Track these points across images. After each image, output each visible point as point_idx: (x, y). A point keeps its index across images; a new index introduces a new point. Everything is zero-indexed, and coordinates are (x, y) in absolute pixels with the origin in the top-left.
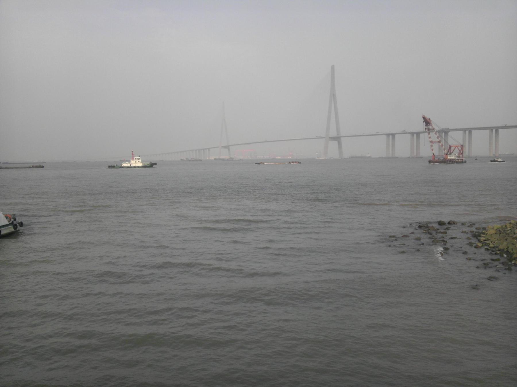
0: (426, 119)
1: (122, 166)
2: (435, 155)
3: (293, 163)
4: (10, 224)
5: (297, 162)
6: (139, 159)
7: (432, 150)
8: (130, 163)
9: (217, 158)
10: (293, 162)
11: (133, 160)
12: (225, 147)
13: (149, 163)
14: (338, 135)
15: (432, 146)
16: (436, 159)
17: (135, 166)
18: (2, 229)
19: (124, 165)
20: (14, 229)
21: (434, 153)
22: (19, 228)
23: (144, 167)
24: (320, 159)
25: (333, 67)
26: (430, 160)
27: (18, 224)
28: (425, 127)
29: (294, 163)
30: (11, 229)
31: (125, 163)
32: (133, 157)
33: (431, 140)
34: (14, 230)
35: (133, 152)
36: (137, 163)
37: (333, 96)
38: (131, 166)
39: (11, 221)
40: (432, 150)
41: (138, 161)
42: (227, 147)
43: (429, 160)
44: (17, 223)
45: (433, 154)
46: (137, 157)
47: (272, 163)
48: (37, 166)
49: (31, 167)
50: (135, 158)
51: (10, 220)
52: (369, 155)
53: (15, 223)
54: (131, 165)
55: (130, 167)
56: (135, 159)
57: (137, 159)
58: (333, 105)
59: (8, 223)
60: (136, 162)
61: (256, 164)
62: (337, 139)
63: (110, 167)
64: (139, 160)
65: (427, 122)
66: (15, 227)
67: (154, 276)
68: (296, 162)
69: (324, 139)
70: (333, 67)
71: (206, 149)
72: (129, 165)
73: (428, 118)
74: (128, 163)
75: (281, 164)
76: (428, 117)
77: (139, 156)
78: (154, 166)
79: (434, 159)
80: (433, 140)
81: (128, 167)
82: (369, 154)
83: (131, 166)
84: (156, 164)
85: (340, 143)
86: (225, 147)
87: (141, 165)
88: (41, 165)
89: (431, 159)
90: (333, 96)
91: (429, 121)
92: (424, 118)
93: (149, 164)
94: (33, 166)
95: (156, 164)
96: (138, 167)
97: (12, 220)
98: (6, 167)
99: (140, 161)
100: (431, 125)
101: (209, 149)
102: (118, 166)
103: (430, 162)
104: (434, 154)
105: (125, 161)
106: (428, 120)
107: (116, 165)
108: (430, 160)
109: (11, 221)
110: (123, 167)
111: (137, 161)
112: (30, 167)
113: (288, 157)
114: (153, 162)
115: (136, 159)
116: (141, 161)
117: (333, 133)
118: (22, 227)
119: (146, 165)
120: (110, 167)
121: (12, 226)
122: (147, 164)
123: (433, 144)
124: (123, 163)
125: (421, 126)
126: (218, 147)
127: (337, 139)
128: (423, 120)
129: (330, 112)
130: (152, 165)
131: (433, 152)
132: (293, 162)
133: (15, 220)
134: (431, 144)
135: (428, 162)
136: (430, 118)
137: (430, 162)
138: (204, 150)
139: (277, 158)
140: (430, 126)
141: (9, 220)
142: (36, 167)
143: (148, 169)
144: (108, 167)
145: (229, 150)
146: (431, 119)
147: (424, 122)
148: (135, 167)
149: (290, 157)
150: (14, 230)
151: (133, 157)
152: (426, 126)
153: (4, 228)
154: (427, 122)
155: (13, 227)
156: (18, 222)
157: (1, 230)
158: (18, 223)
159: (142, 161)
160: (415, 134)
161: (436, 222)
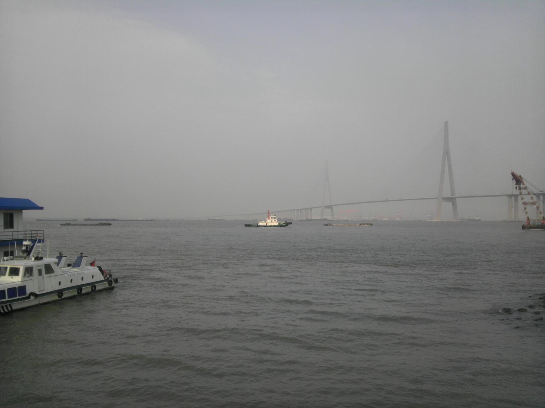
0: (515, 176)
1: (259, 225)
2: (530, 219)
3: (364, 225)
4: (105, 280)
5: (369, 224)
6: (275, 218)
7: (527, 213)
8: (265, 222)
9: (320, 218)
10: (364, 224)
11: (269, 219)
12: (327, 207)
13: (284, 222)
14: (452, 195)
15: (525, 208)
16: (532, 224)
17: (271, 225)
18: (97, 284)
19: (261, 224)
20: (109, 285)
21: (529, 217)
22: (114, 284)
23: (280, 226)
24: (433, 221)
25: (446, 123)
26: (524, 225)
27: (113, 281)
28: (515, 186)
29: (365, 225)
30: (106, 285)
31: (261, 222)
32: (269, 216)
33: (523, 201)
34: (109, 286)
35: (269, 211)
36: (272, 222)
37: (447, 153)
38: (267, 225)
39: (107, 277)
40: (527, 213)
41: (274, 221)
42: (330, 207)
43: (522, 225)
44: (112, 279)
45: (527, 219)
46: (273, 216)
47: (341, 225)
48: (105, 223)
49: (99, 224)
50: (271, 217)
51: (106, 276)
52: (478, 218)
53: (110, 279)
54: (266, 224)
55: (266, 226)
56: (271, 218)
57: (273, 218)
58: (446, 162)
59: (103, 279)
60: (271, 221)
61: (61, 225)
62: (452, 200)
63: (247, 226)
64: (274, 219)
65: (518, 180)
66: (110, 283)
67: (360, 338)
68: (367, 224)
69: (437, 199)
70: (446, 123)
71: (308, 209)
72: (264, 224)
73: (519, 176)
74: (264, 222)
75: (351, 226)
76: (518, 173)
77: (275, 215)
78: (289, 225)
79: (529, 224)
80: (526, 202)
81: (264, 226)
82: (478, 217)
83: (267, 225)
84: (291, 223)
85: (454, 205)
86: (327, 207)
87: (277, 224)
88: (109, 222)
89: (525, 224)
90: (447, 153)
91: (520, 179)
92: (513, 174)
93: (284, 224)
94: (100, 223)
95: (291, 223)
96: (274, 226)
97: (108, 276)
98: (75, 224)
99: (276, 221)
100: (523, 184)
101: (311, 209)
102: (255, 225)
103: (524, 227)
104: (528, 218)
105: (262, 221)
106: (518, 178)
107: (253, 224)
108: (524, 225)
109: (107, 277)
110: (260, 226)
111: (273, 220)
112: (97, 225)
113: (397, 219)
114: (288, 222)
115: (271, 218)
116: (276, 220)
117: (447, 193)
118: (117, 283)
119: (282, 224)
120: (247, 226)
121: (107, 282)
122: (282, 223)
123: (527, 206)
124: (259, 222)
125: (510, 186)
126: (321, 207)
127: (452, 200)
128: (512, 177)
129: (443, 172)
130: (287, 224)
131: (528, 215)
132: (364, 224)
133: (111, 276)
134: (524, 206)
135: (521, 228)
136: (521, 175)
137: (524, 227)
138: (305, 209)
139: (383, 219)
140: (522, 185)
141: (105, 276)
142: (104, 224)
143: (283, 228)
144: (244, 226)
145: (332, 210)
146: (523, 176)
147: (513, 180)
148: (271, 226)
149: (399, 219)
150: (109, 286)
151: (269, 216)
152: (516, 184)
153: (100, 284)
154: (518, 180)
155: (108, 284)
156: (113, 278)
157: (96, 286)
158: (113, 280)
159: (277, 220)
160: (541, 195)
161: (527, 306)
